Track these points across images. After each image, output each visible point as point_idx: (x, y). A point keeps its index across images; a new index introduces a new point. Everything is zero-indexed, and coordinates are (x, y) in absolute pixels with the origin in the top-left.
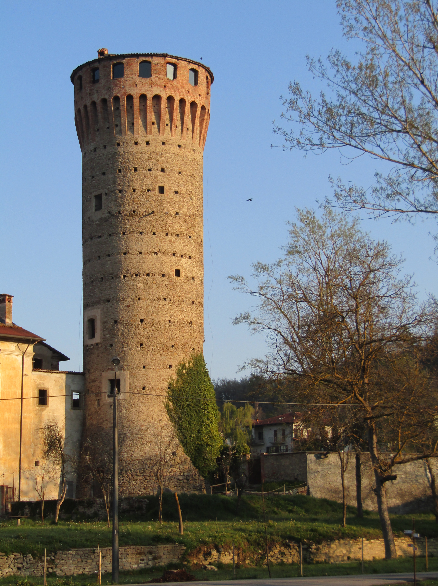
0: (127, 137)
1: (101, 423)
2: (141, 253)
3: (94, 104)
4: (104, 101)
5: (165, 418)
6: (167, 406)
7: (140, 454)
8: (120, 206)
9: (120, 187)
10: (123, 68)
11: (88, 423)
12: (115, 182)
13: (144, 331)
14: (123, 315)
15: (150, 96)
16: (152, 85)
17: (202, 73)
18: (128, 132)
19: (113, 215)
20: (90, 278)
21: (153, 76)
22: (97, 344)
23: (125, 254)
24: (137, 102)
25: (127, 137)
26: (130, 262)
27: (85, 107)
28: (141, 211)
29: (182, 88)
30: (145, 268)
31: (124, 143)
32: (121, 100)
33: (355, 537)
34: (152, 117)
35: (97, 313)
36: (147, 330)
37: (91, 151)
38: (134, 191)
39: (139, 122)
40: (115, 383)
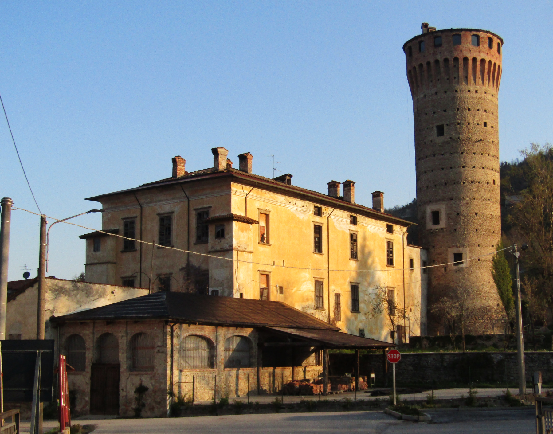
0: (463, 86)
1: (449, 283)
2: (474, 167)
4: (421, 65)
5: (492, 280)
6: (492, 272)
7: (480, 305)
8: (459, 134)
9: (459, 121)
10: (461, 38)
11: (435, 283)
12: (455, 117)
13: (478, 220)
15: (479, 59)
16: (480, 52)
18: (464, 83)
19: (454, 140)
20: (434, 183)
21: (481, 46)
22: (442, 229)
23: (463, 167)
24: (470, 62)
25: (463, 86)
26: (468, 173)
27: (429, 63)
28: (474, 138)
30: (477, 178)
31: (460, 91)
32: (460, 60)
36: (480, 221)
37: (432, 94)
38: (469, 124)
39: (471, 78)
40: (458, 257)
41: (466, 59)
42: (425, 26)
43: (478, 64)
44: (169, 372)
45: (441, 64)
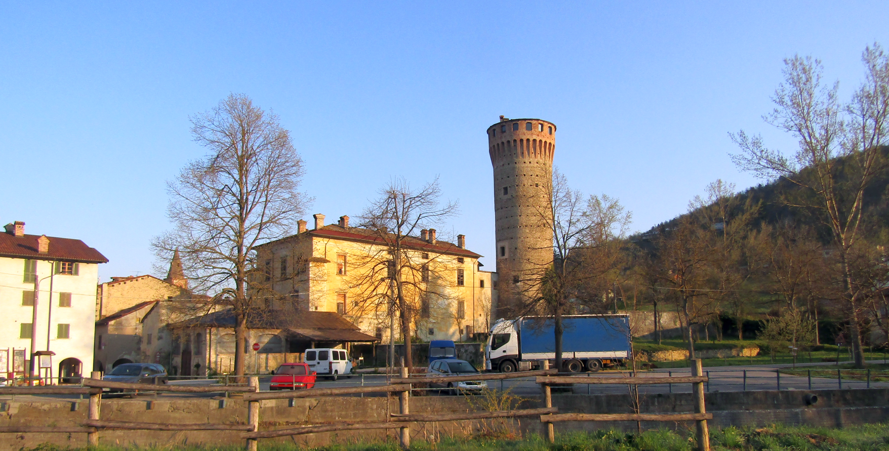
3: (503, 143)
4: (509, 142)
14: (520, 245)
15: (531, 140)
17: (552, 128)
24: (525, 142)
29: (545, 137)
33: (667, 350)
34: (532, 150)
35: (506, 244)
41: (522, 140)
42: (501, 118)
43: (531, 143)
44: (208, 356)
45: (506, 145)
